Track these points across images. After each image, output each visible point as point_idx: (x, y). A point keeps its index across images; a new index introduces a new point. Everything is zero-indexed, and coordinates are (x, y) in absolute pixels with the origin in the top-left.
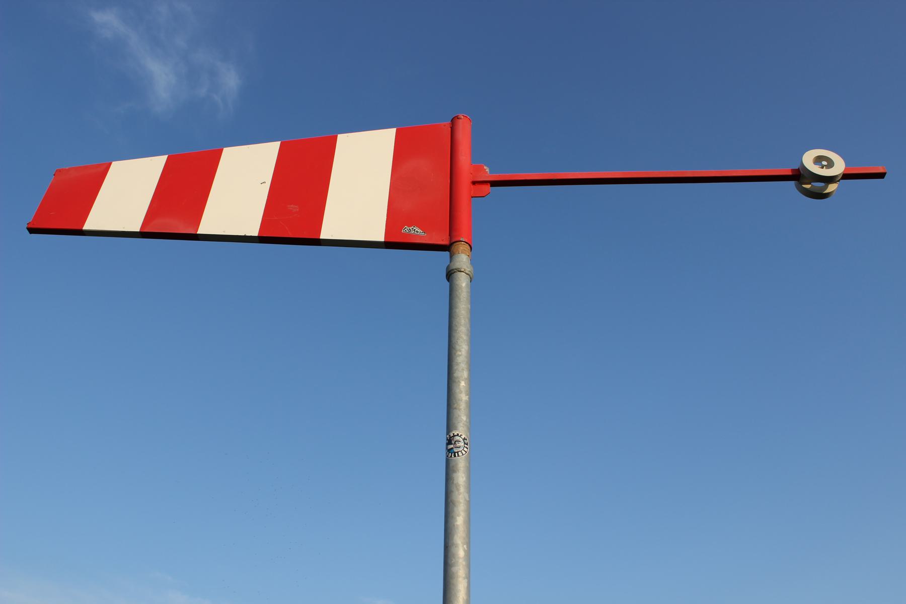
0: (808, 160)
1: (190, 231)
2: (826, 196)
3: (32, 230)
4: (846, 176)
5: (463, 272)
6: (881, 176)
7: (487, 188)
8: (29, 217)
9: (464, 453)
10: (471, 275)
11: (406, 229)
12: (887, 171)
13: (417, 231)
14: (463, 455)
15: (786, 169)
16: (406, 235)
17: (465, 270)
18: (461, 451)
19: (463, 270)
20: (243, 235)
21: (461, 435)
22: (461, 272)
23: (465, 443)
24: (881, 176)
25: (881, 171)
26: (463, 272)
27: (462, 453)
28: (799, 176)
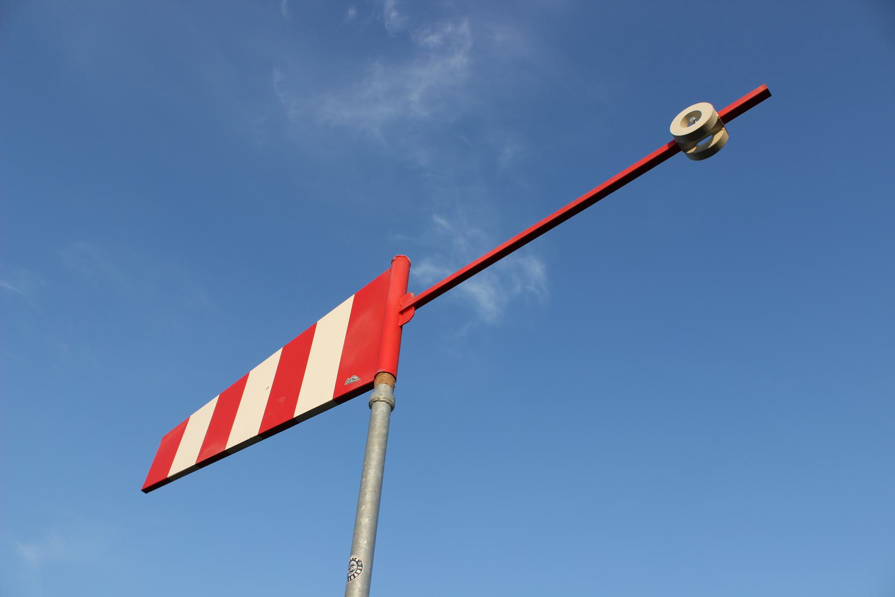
0: (679, 128)
1: (286, 419)
2: (715, 149)
3: (147, 490)
4: (725, 119)
5: (377, 401)
6: (765, 94)
7: (411, 312)
8: (142, 483)
9: (358, 571)
10: (386, 400)
11: (349, 381)
12: (767, 87)
13: (355, 379)
14: (361, 570)
15: (664, 148)
16: (350, 385)
17: (379, 399)
18: (353, 575)
19: (377, 399)
20: (249, 438)
21: (356, 559)
22: (375, 401)
23: (358, 565)
24: (765, 94)
25: (761, 89)
26: (377, 401)
27: (357, 573)
28: (677, 146)
